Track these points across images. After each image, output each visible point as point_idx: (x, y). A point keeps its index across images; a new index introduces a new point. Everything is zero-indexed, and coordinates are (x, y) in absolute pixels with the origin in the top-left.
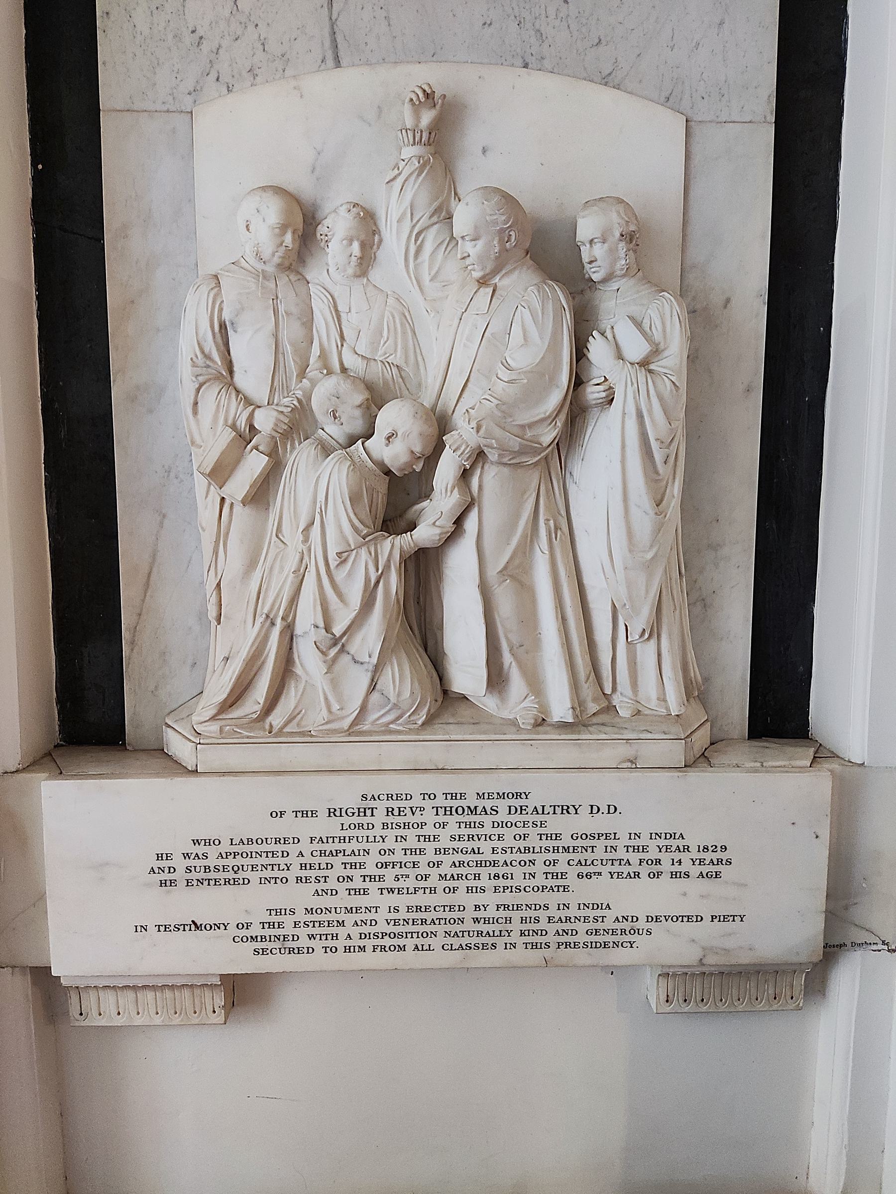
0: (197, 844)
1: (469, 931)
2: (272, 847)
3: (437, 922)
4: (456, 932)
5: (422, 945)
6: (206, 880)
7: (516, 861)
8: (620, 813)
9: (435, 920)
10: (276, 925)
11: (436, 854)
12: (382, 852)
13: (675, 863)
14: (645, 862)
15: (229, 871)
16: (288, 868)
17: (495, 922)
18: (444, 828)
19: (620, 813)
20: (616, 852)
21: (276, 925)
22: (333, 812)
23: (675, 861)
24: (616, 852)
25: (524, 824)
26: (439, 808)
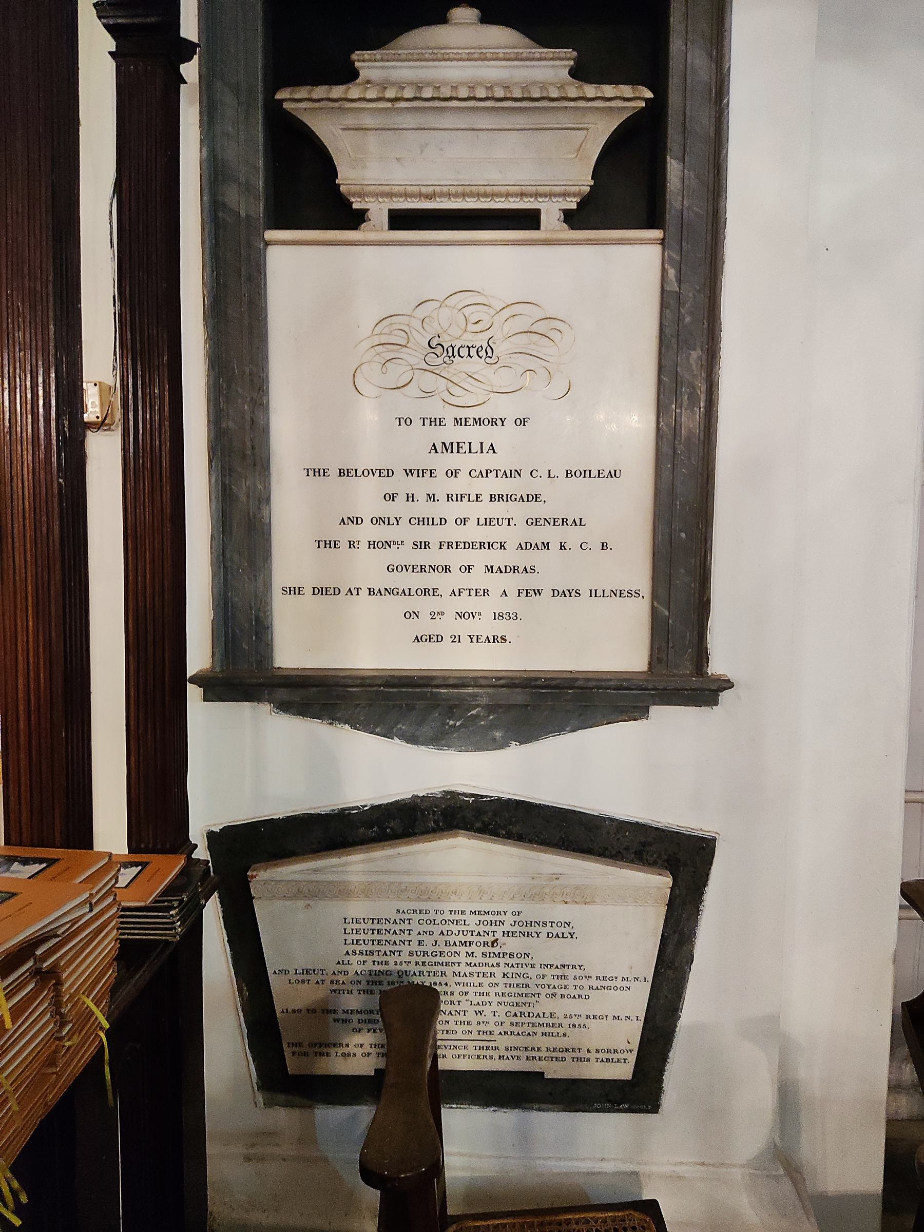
14: (474, 944)
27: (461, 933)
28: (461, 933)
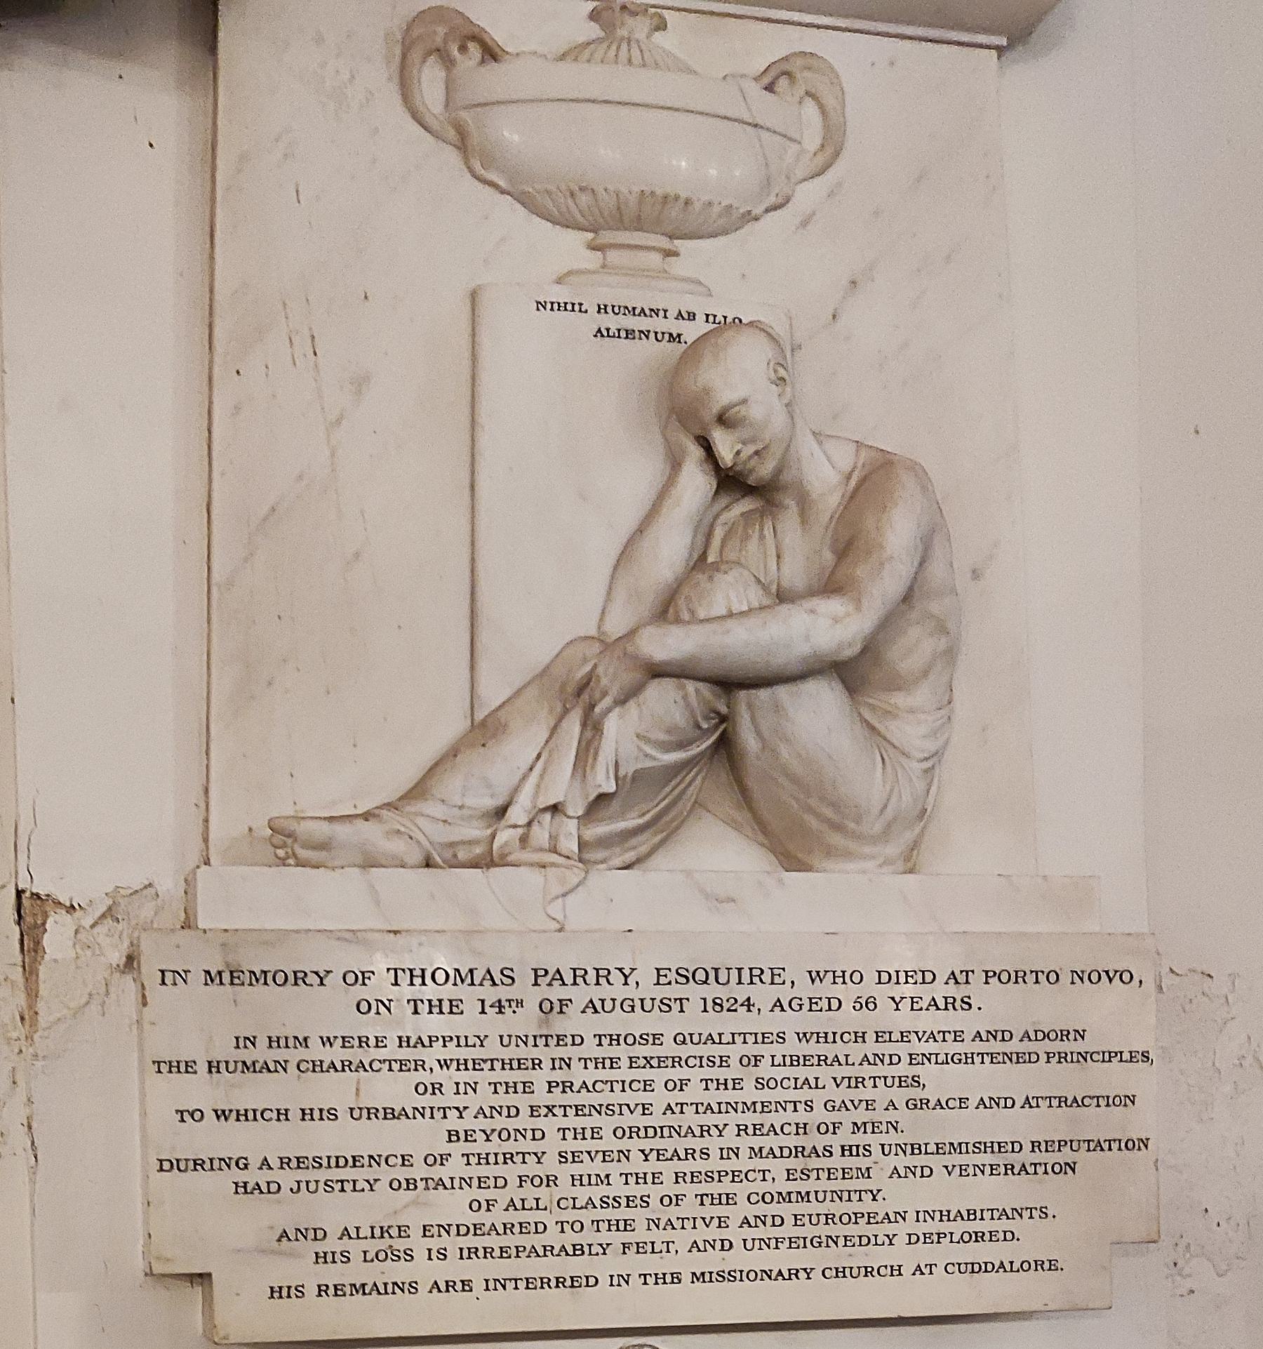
0: (445, 1067)
1: (885, 1078)
2: (477, 1270)
3: (939, 1037)
4: (932, 1033)
5: (847, 1056)
6: (1027, 1209)
7: (757, 1194)
8: (980, 1009)
9: (673, 1106)
10: (588, 1134)
11: (450, 1141)
12: (364, 1007)
13: (487, 1009)
15: (804, 1225)
16: (891, 1240)
17: (659, 1130)
18: (442, 1164)
19: (980, 1009)
20: (379, 1166)
21: (588, 1134)
22: (759, 976)
23: (487, 1004)
24: (379, 1166)
25: (645, 1085)
26: (568, 1108)
27: (303, 1185)
28: (303, 1185)
